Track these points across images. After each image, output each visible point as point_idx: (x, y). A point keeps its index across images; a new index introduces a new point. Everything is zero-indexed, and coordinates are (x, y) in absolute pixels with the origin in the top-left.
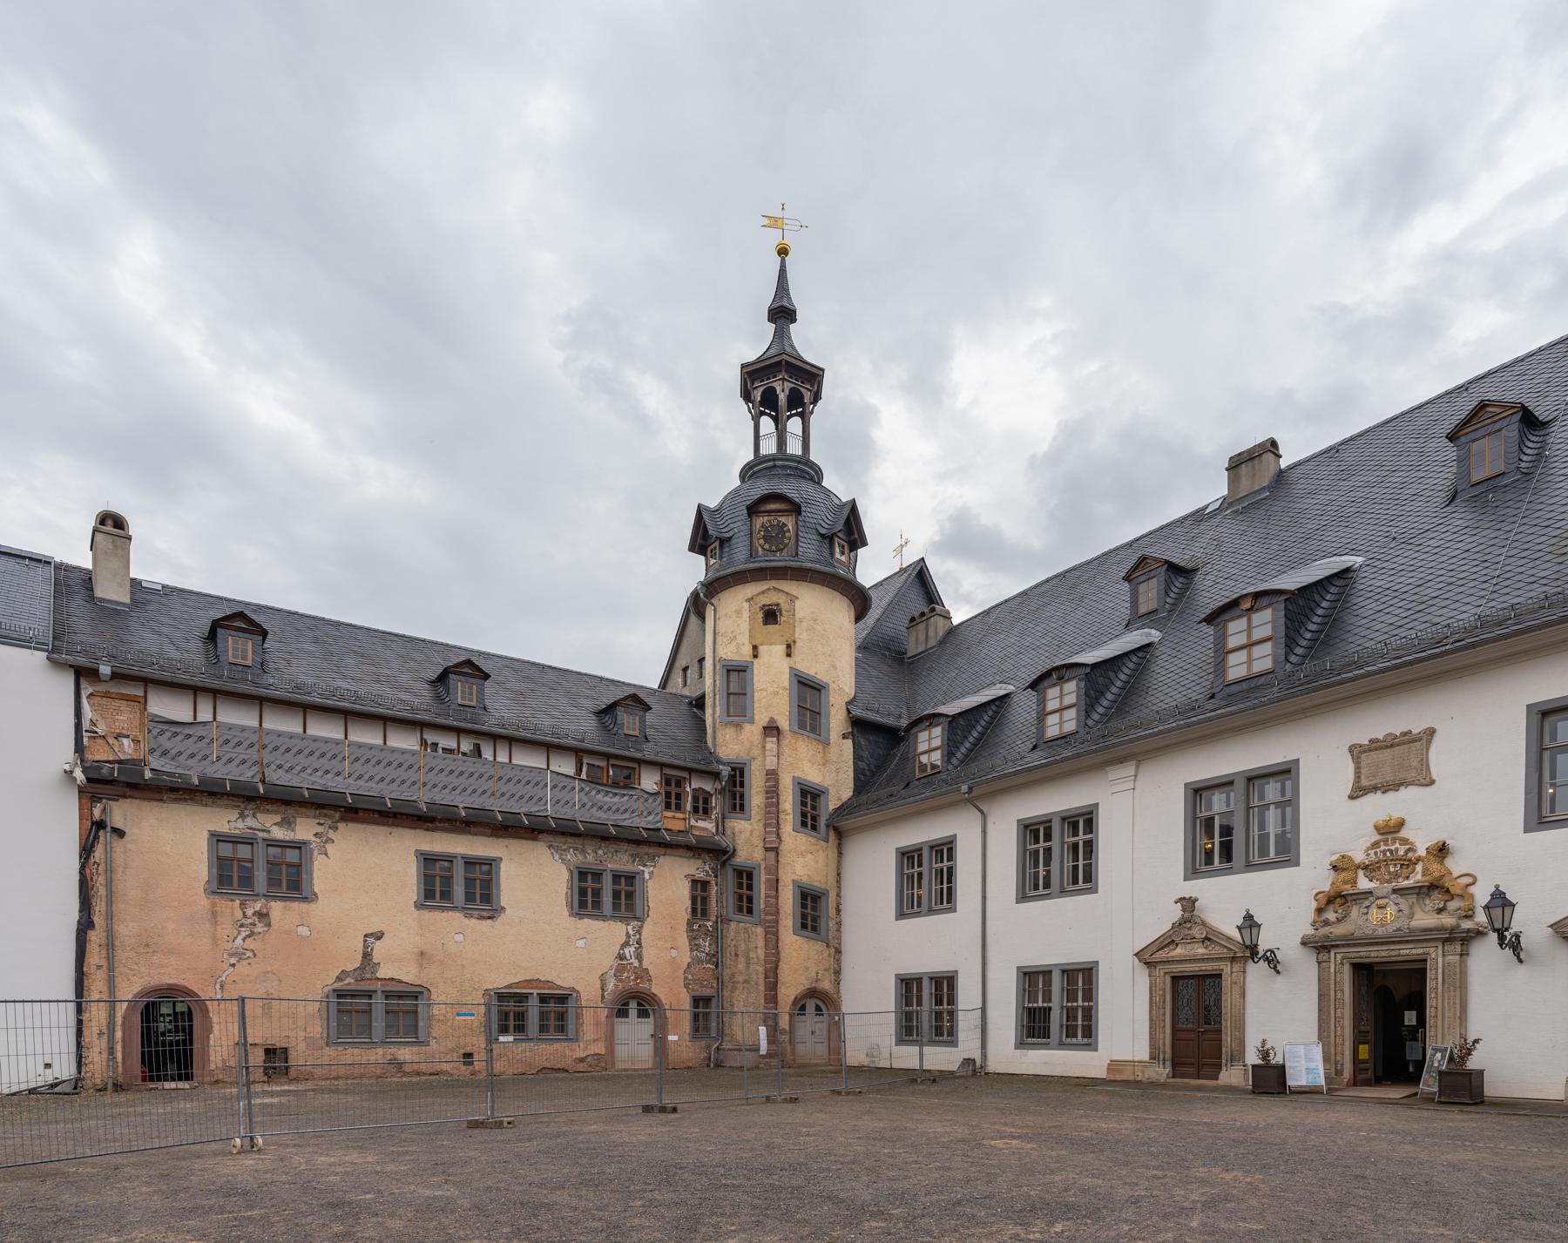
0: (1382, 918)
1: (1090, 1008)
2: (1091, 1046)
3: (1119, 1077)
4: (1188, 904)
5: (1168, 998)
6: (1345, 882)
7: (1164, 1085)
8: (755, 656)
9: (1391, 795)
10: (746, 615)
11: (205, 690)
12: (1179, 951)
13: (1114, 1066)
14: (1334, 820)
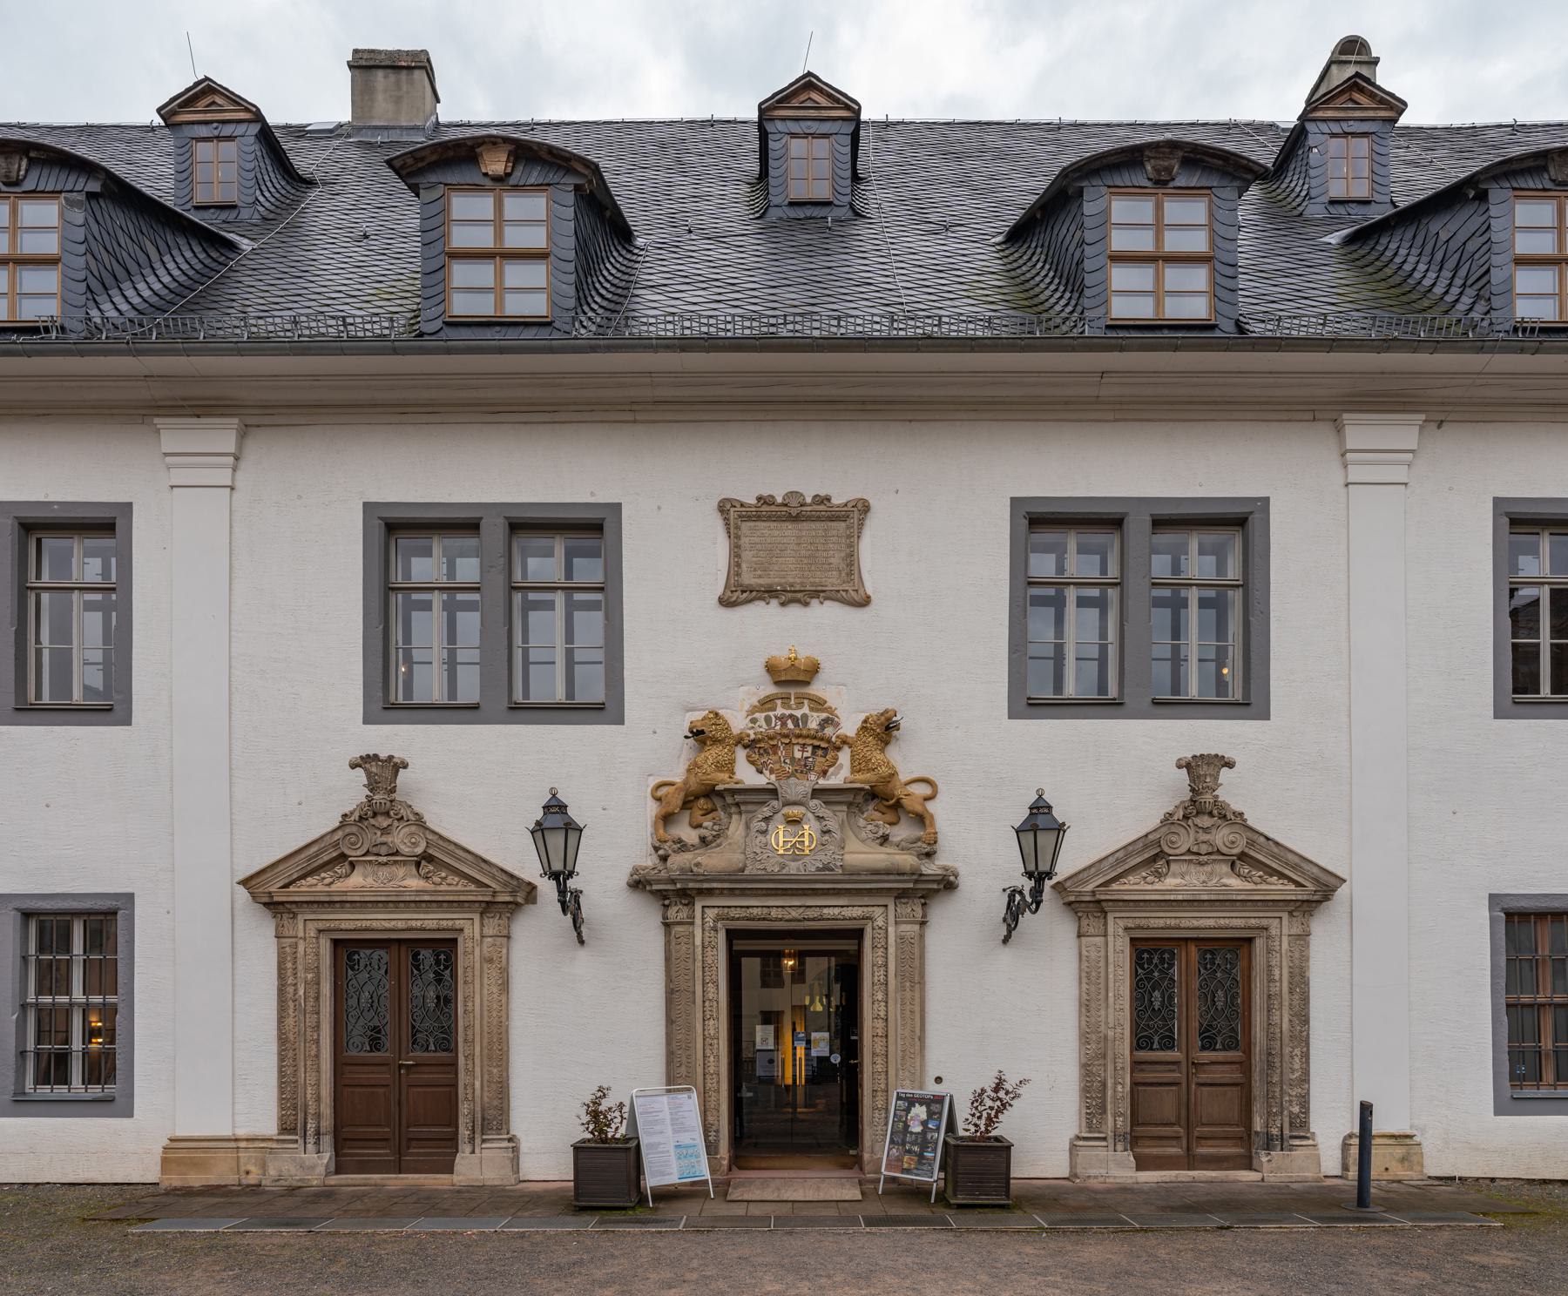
0: (787, 842)
1: (109, 1012)
2: (118, 1105)
3: (196, 1180)
4: (382, 772)
5: (326, 989)
6: (720, 767)
7: (326, 1195)
9: (795, 611)
12: (357, 881)
13: (178, 1151)
14: (689, 647)
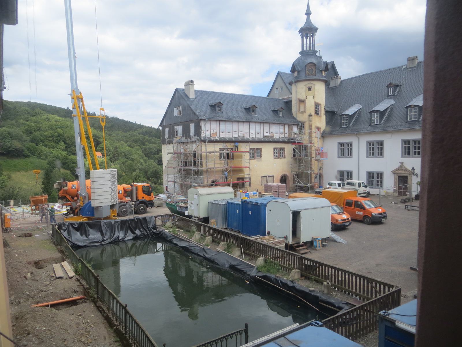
1: (382, 181)
4: (402, 163)
8: (306, 98)
10: (304, 89)
11: (222, 121)
13: (387, 193)
